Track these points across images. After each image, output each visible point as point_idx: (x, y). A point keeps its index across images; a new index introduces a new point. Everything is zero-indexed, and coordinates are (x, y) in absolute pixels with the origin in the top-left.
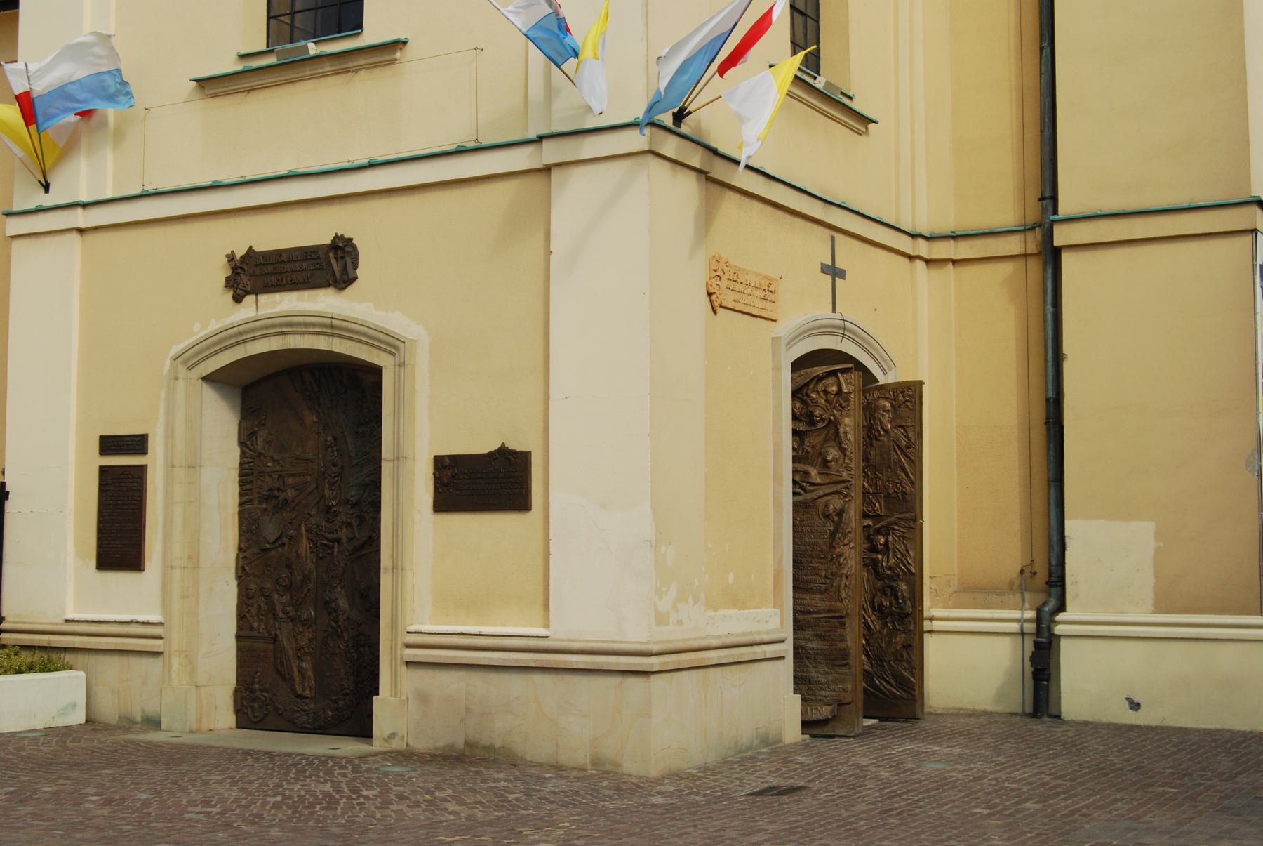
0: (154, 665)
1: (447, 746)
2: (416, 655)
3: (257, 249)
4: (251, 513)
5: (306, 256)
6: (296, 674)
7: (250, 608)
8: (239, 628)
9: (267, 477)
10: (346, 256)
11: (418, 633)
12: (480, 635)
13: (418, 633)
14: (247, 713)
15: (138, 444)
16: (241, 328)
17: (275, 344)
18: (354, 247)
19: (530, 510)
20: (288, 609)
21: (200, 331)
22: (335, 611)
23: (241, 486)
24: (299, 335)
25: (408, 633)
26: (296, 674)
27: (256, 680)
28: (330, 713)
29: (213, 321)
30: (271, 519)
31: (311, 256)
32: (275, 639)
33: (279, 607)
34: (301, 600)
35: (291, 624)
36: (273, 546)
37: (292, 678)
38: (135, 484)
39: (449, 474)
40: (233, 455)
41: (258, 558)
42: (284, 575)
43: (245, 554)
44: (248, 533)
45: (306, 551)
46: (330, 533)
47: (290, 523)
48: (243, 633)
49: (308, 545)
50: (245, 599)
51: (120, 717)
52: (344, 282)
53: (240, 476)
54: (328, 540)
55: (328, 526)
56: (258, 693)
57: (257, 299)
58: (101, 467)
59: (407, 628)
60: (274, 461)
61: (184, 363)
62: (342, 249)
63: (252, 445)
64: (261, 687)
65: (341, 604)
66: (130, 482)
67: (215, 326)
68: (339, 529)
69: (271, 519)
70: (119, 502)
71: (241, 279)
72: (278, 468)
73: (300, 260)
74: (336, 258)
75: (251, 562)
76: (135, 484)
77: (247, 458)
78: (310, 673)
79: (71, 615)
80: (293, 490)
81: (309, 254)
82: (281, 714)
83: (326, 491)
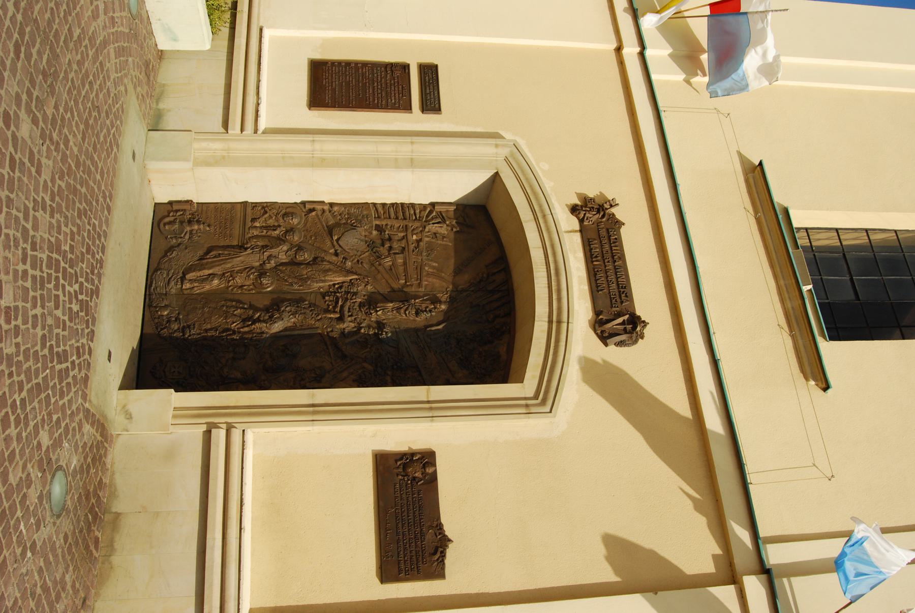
0: (218, 126)
1: (116, 490)
2: (218, 446)
3: (623, 230)
4: (367, 218)
5: (622, 287)
6: (207, 272)
7: (274, 218)
8: (255, 205)
9: (402, 234)
10: (628, 335)
11: (243, 445)
12: (241, 529)
13: (243, 445)
14: (168, 216)
15: (431, 104)
16: (550, 217)
17: (536, 255)
18: (636, 342)
19: (382, 582)
20: (273, 262)
21: (541, 168)
22: (271, 317)
23: (393, 204)
24: (547, 282)
25: (244, 431)
26: (207, 272)
27: (202, 226)
28: (166, 313)
29: (552, 184)
30: (362, 240)
31: (623, 293)
32: (242, 247)
33: (274, 251)
34: (282, 275)
35: (257, 264)
36: (335, 243)
37: (202, 267)
38: (393, 101)
39: (417, 475)
40: (422, 197)
41: (323, 226)
42: (306, 256)
43: (328, 212)
44: (348, 214)
45: (331, 281)
46: (349, 309)
47: (358, 261)
48: (249, 210)
49: (336, 282)
50: (284, 211)
51: (164, 85)
52: (602, 332)
53: (402, 204)
54: (342, 307)
55: (357, 304)
56: (188, 229)
57: (576, 231)
58: (408, 65)
59: (249, 430)
60: (418, 241)
61: (512, 155)
62: (634, 328)
63: (432, 219)
64: (195, 232)
65: (276, 325)
66: (395, 94)
67: (548, 185)
68: (353, 318)
69: (362, 240)
70: (376, 85)
71: (595, 214)
72: (412, 247)
73: (618, 282)
74: (623, 323)
75: (319, 219)
76: (393, 101)
77: (420, 212)
78: (207, 287)
79: (267, 33)
80: (391, 263)
81: (624, 291)
82: (165, 255)
83: (391, 305)
